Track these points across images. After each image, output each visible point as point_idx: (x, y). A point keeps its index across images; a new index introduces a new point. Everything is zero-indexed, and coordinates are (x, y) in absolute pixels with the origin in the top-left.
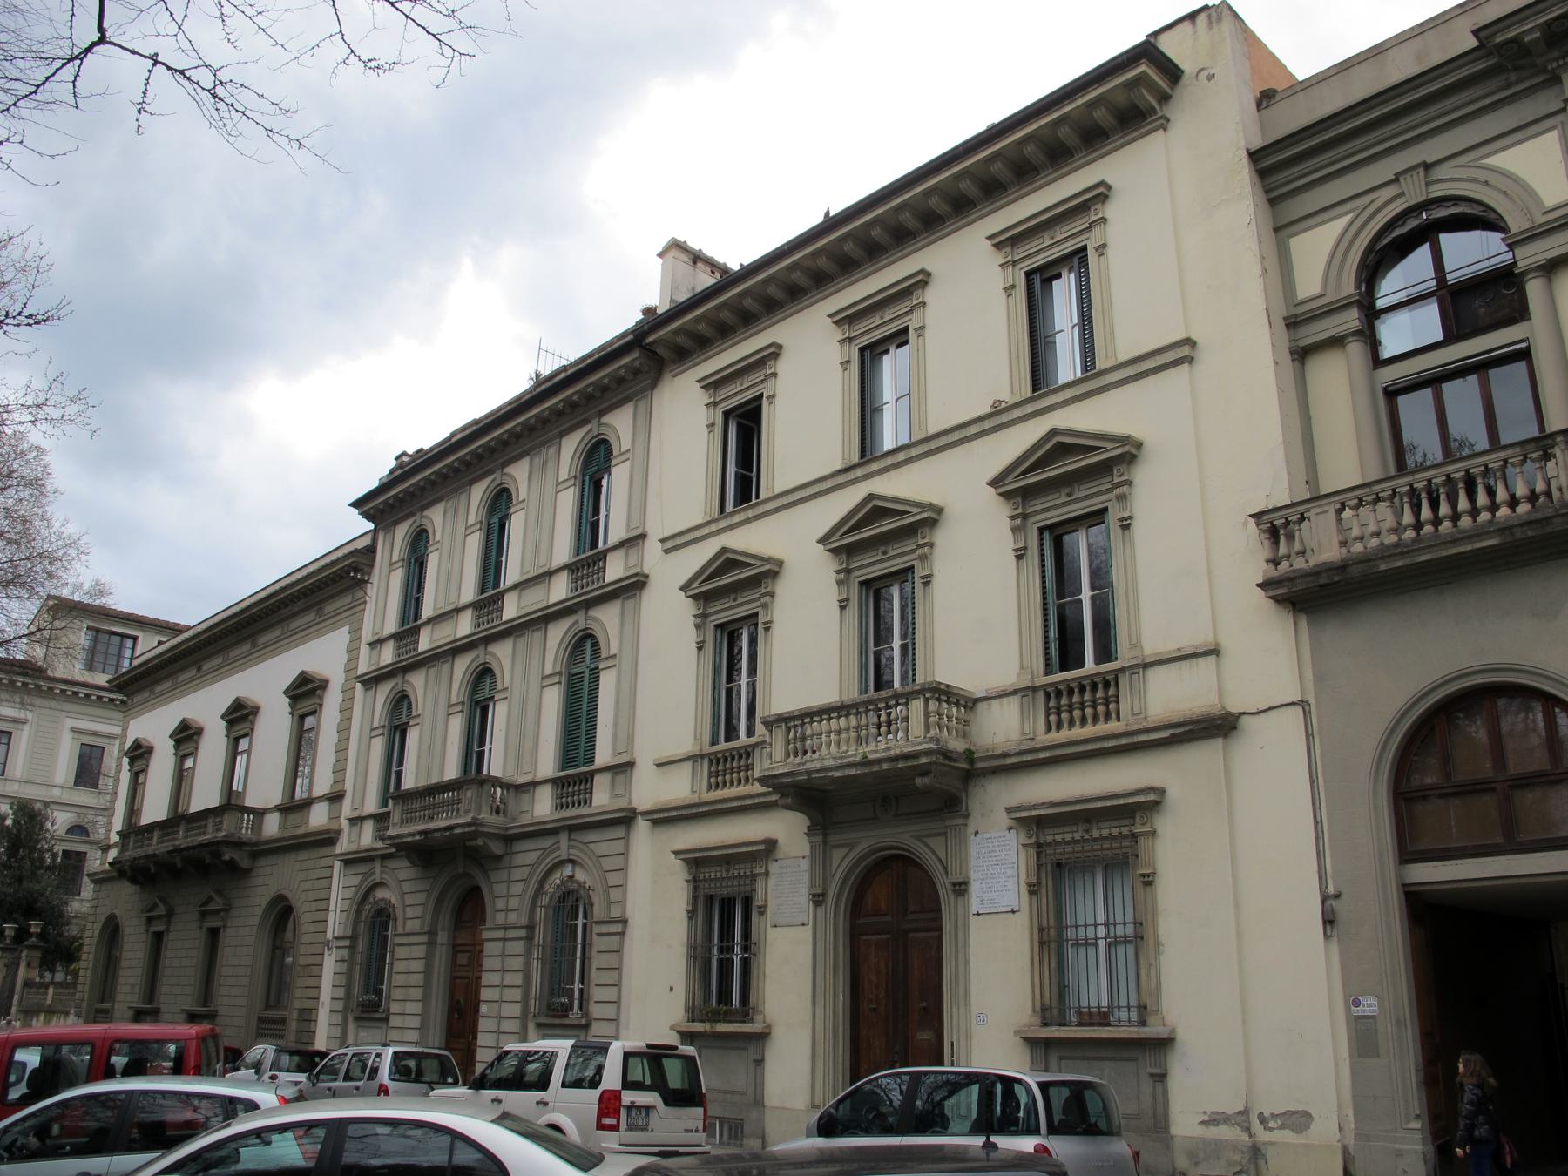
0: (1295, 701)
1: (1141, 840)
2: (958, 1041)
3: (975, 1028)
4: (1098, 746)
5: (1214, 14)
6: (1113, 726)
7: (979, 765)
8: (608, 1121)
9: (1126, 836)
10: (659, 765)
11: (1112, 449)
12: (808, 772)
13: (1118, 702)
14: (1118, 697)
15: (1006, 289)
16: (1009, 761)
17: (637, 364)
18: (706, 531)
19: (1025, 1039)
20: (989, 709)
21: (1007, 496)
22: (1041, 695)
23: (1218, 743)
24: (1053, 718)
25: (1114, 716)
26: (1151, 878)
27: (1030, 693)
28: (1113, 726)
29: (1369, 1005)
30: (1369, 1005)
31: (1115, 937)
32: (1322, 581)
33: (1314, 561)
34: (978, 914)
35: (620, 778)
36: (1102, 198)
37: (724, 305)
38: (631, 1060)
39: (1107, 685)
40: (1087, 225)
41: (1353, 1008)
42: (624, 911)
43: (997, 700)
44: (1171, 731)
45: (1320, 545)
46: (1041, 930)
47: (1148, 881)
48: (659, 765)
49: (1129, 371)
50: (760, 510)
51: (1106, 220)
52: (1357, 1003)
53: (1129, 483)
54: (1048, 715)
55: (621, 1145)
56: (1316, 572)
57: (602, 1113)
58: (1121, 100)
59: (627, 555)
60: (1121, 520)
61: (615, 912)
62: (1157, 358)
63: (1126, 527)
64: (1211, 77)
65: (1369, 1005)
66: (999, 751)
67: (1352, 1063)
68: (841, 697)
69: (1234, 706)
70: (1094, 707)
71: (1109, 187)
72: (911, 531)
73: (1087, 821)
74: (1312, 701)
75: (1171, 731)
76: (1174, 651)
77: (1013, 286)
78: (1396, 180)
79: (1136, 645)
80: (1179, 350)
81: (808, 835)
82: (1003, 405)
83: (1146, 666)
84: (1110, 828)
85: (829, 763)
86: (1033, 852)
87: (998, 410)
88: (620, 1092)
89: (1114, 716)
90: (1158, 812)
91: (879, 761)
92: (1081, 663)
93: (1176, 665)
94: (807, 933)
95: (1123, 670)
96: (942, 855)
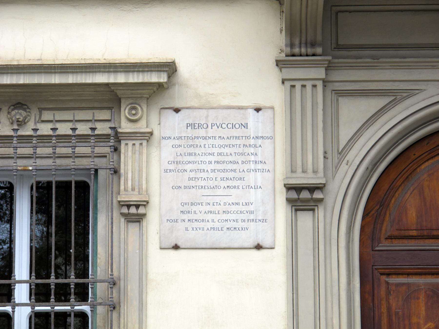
9: (105, 137)
81: (278, 63)
90: (256, 108)
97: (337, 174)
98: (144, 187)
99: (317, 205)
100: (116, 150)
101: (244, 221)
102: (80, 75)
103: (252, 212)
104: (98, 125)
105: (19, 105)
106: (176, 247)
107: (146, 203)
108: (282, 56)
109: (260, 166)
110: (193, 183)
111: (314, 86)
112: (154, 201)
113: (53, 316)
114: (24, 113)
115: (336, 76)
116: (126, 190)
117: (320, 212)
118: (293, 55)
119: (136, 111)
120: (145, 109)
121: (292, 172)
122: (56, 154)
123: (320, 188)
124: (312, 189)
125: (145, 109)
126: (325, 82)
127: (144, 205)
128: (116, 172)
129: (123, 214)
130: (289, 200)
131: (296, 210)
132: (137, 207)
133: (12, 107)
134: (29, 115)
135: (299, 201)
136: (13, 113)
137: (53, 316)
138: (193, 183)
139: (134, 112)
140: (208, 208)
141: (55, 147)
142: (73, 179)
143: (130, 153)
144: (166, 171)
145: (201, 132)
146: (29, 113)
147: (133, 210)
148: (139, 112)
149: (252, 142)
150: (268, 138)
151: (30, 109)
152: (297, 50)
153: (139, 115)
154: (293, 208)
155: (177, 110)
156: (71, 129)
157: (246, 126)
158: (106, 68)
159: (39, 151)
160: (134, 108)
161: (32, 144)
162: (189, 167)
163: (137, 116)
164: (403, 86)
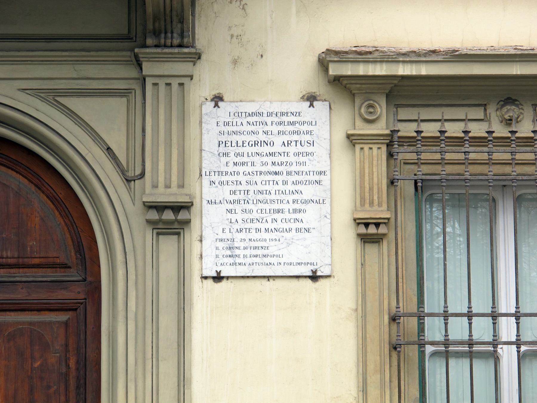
34: (218, 278)
97: (115, 191)
99: (183, 228)
102: (424, 65)
104: (424, 127)
105: (509, 101)
114: (516, 109)
119: (374, 110)
122: (445, 160)
127: (385, 223)
131: (158, 234)
132: (377, 225)
133: (502, 103)
134: (521, 113)
135: (161, 223)
136: (505, 109)
139: (371, 110)
146: (521, 111)
148: (364, 110)
151: (522, 105)
153: (379, 113)
154: (155, 231)
156: (532, 131)
158: (516, 57)
161: (533, 148)
163: (376, 115)
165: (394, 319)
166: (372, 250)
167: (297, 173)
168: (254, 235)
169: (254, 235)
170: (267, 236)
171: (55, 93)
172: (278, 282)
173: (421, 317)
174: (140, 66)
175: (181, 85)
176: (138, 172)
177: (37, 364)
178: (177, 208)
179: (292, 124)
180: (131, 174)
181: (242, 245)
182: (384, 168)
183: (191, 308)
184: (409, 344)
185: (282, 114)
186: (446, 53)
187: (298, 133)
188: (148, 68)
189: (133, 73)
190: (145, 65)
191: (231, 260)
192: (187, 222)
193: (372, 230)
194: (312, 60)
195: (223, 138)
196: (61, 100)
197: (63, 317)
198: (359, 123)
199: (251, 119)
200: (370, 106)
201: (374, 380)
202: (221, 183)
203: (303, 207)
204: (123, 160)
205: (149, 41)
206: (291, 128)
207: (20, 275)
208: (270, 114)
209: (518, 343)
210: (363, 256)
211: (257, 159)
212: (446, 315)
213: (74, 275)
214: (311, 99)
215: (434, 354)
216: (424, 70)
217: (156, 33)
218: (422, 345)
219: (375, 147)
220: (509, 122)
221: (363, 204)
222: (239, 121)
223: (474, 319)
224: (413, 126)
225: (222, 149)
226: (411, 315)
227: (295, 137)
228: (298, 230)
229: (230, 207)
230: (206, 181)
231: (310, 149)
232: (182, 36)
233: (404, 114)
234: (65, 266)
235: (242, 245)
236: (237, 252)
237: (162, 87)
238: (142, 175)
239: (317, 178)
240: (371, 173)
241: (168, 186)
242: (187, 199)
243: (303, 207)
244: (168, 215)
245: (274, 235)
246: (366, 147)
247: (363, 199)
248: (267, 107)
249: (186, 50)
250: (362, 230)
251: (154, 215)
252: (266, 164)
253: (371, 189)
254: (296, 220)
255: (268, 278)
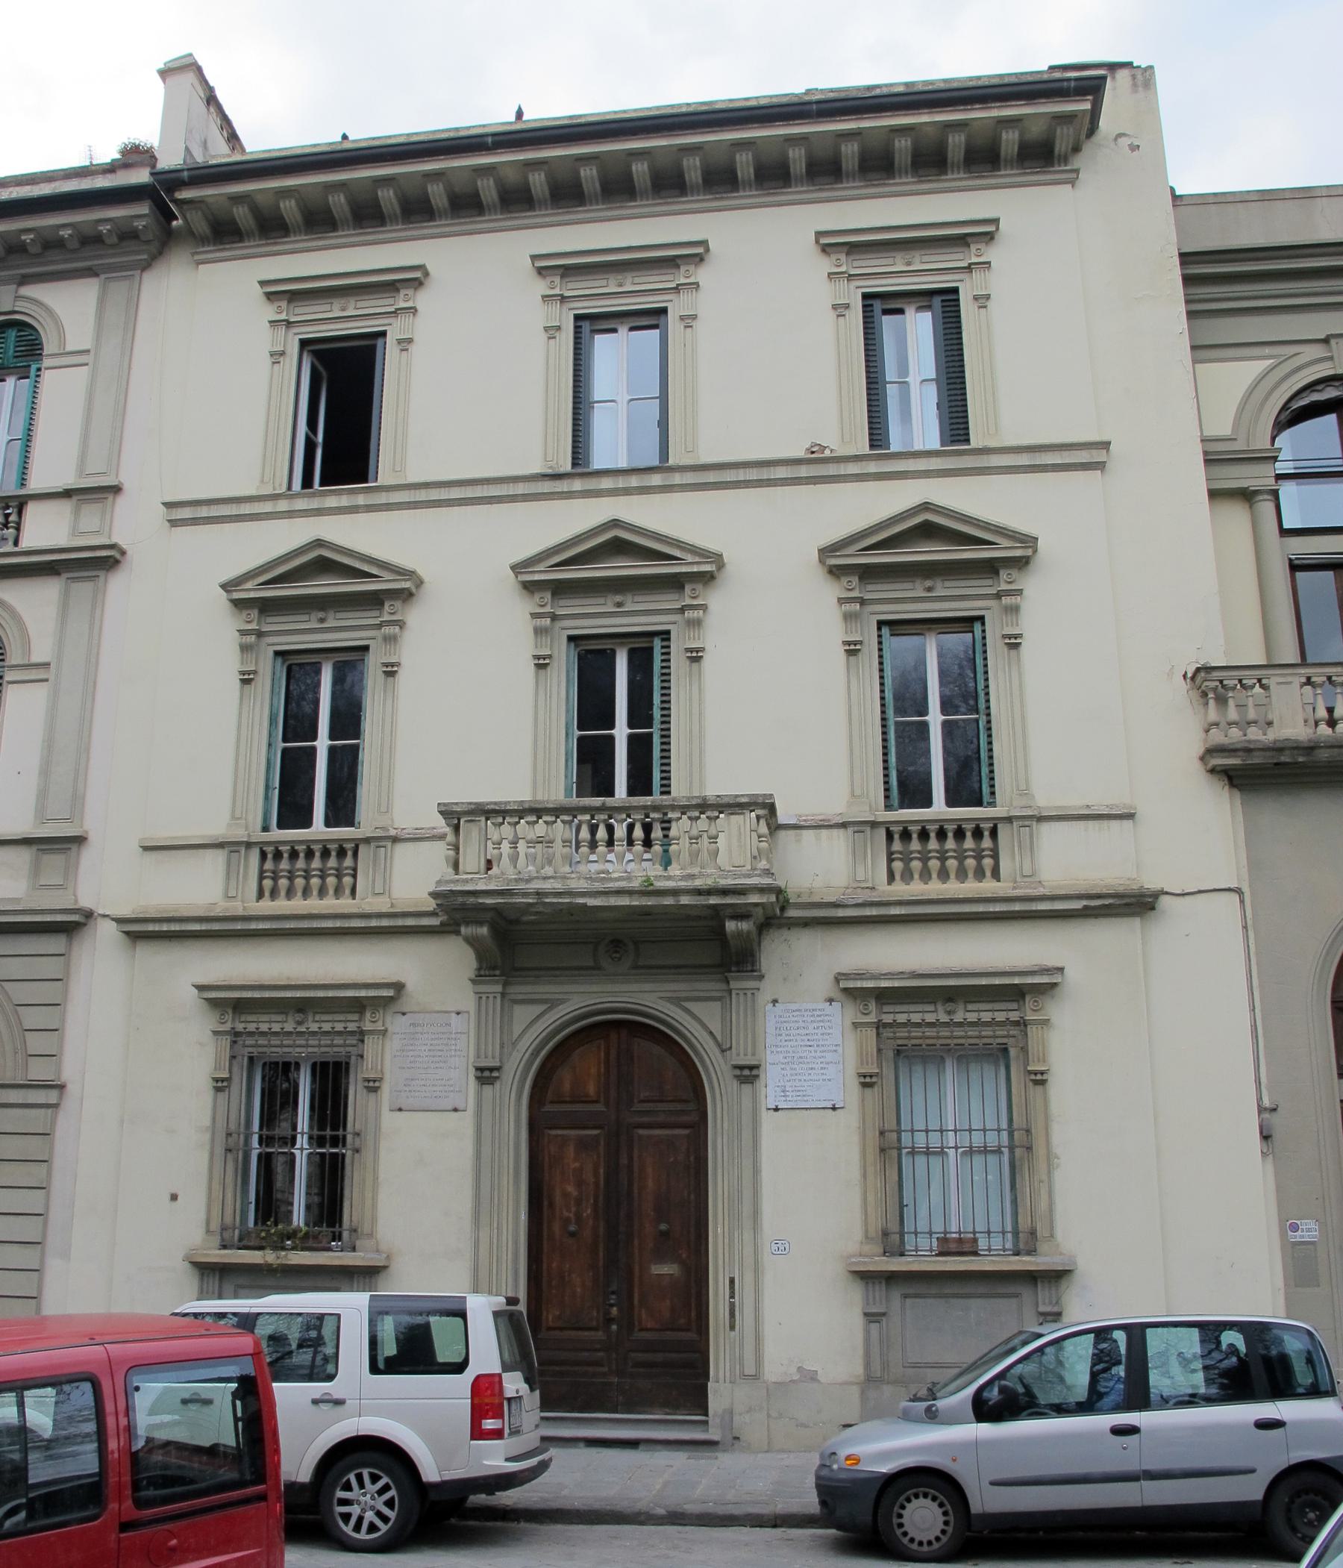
0: (1232, 886)
1: (1032, 1031)
2: (742, 1276)
3: (767, 1259)
4: (980, 908)
5: (1139, 77)
6: (988, 887)
7: (792, 913)
8: (489, 1424)
9: (352, 1033)
10: (146, 849)
11: (1006, 548)
12: (538, 894)
13: (354, 876)
14: (355, 869)
15: (272, 354)
16: (841, 913)
17: (140, 224)
18: (267, 507)
19: (195, 1264)
20: (799, 841)
21: (239, 604)
22: (255, 856)
23: (1136, 922)
24: (268, 883)
25: (988, 873)
26: (377, 1084)
27: (243, 850)
28: (988, 887)
29: (1309, 1230)
30: (1309, 1230)
31: (971, 1147)
32: (1283, 759)
33: (1271, 736)
34: (776, 1109)
35: (54, 861)
36: (698, 259)
37: (342, 185)
38: (336, 1317)
39: (342, 853)
40: (392, 309)
41: (1290, 1233)
42: (59, 1071)
43: (811, 832)
44: (1085, 903)
45: (1281, 718)
46: (229, 1135)
47: (1039, 1080)
48: (146, 849)
49: (1024, 460)
50: (382, 498)
51: (416, 311)
52: (1295, 1228)
53: (401, 624)
54: (890, 860)
55: (507, 1460)
56: (1278, 748)
57: (479, 1412)
58: (512, 176)
59: (77, 513)
60: (386, 665)
61: (38, 1071)
62: (1065, 454)
63: (390, 674)
64: (1134, 148)
65: (1309, 1230)
66: (816, 899)
67: (1286, 1293)
68: (534, 793)
69: (1151, 883)
70: (323, 877)
71: (427, 274)
72: (375, 600)
73: (300, 1011)
74: (1246, 889)
75: (1085, 903)
76: (1081, 808)
77: (282, 354)
78: (1326, 341)
79: (1026, 793)
80: (1094, 452)
81: (473, 982)
82: (827, 453)
83: (395, 840)
84: (270, 1022)
85: (582, 885)
86: (226, 1041)
87: (816, 456)
88: (500, 1375)
89: (348, 891)
90: (1053, 997)
91: (675, 892)
92: (306, 822)
93: (1081, 824)
94: (465, 1123)
95: (367, 841)
96: (716, 1027)
98: (379, 1067)
100: (363, 1041)
101: (446, 1092)
103: (452, 1086)
105: (950, 1000)
106: (400, 1110)
107: (381, 1080)
108: (473, 977)
109: (458, 1053)
110: (413, 1065)
111: (495, 997)
112: (387, 1077)
113: (327, 1157)
115: (511, 989)
116: (367, 1069)
117: (497, 1085)
118: (481, 976)
120: (381, 1012)
121: (478, 1057)
123: (498, 1069)
124: (491, 1070)
125: (381, 1012)
126: (503, 995)
128: (362, 1056)
129: (365, 1087)
130: (477, 1078)
131: (741, 1083)
137: (327, 1157)
138: (413, 1065)
140: (423, 1082)
141: (320, 1040)
142: (331, 1060)
143: (371, 1045)
144: (395, 1056)
145: (419, 1029)
147: (371, 1084)
149: (453, 1036)
150: (464, 1033)
152: (482, 973)
155: (404, 1014)
157: (450, 1025)
159: (310, 1042)
160: (374, 1013)
162: (412, 1053)
164: (557, 996)
165: (882, 1133)
166: (868, 1091)
167: (823, 1046)
168: (797, 1083)
169: (797, 1083)
170: (805, 1084)
171: (679, 999)
172: (812, 1111)
173: (899, 1132)
174: (728, 982)
175: (753, 994)
176: (728, 1046)
177: (672, 1160)
178: (751, 1068)
179: (820, 1016)
180: (724, 1047)
181: (790, 1089)
182: (1030, 1042)
183: (761, 1127)
184: (890, 1148)
185: (813, 1010)
186: (909, 973)
187: (822, 1021)
188: (733, 985)
189: (724, 986)
190: (731, 982)
191: (784, 1099)
192: (757, 1076)
193: (868, 1080)
194: (831, 977)
195: (778, 1025)
196: (683, 1003)
197: (686, 1132)
198: (859, 1015)
199: (795, 1014)
200: (866, 1005)
201: (870, 1170)
202: (777, 1052)
203: (826, 1066)
204: (719, 1038)
205: (733, 969)
206: (819, 1019)
207: (661, 1107)
208: (806, 1010)
209: (956, 1148)
210: (863, 1095)
211: (798, 1038)
212: (912, 1131)
213: (691, 1106)
214: (831, 1000)
215: (908, 1153)
216: (897, 984)
217: (738, 964)
218: (899, 1149)
219: (869, 1029)
220: (949, 1013)
221: (862, 1064)
222: (788, 1015)
223: (973, 1132)
224: (255, 1025)
225: (778, 1032)
226: (892, 1131)
227: (822, 1024)
228: (824, 1080)
229: (783, 1066)
230: (768, 1052)
231: (830, 1031)
232: (753, 966)
233: (886, 1008)
234: (686, 1101)
235: (790, 1089)
236: (788, 1093)
237: (742, 997)
238: (731, 1048)
239: (834, 1048)
240: (867, 1046)
241: (745, 1055)
242: (756, 1063)
243: (826, 1066)
244: (746, 1072)
245: (809, 1083)
246: (864, 1029)
247: (862, 1061)
248: (805, 1006)
249: (755, 974)
250: (862, 1080)
251: (738, 1072)
252: (803, 1040)
253: (867, 1054)
254: (823, 1074)
255: (807, 1109)
